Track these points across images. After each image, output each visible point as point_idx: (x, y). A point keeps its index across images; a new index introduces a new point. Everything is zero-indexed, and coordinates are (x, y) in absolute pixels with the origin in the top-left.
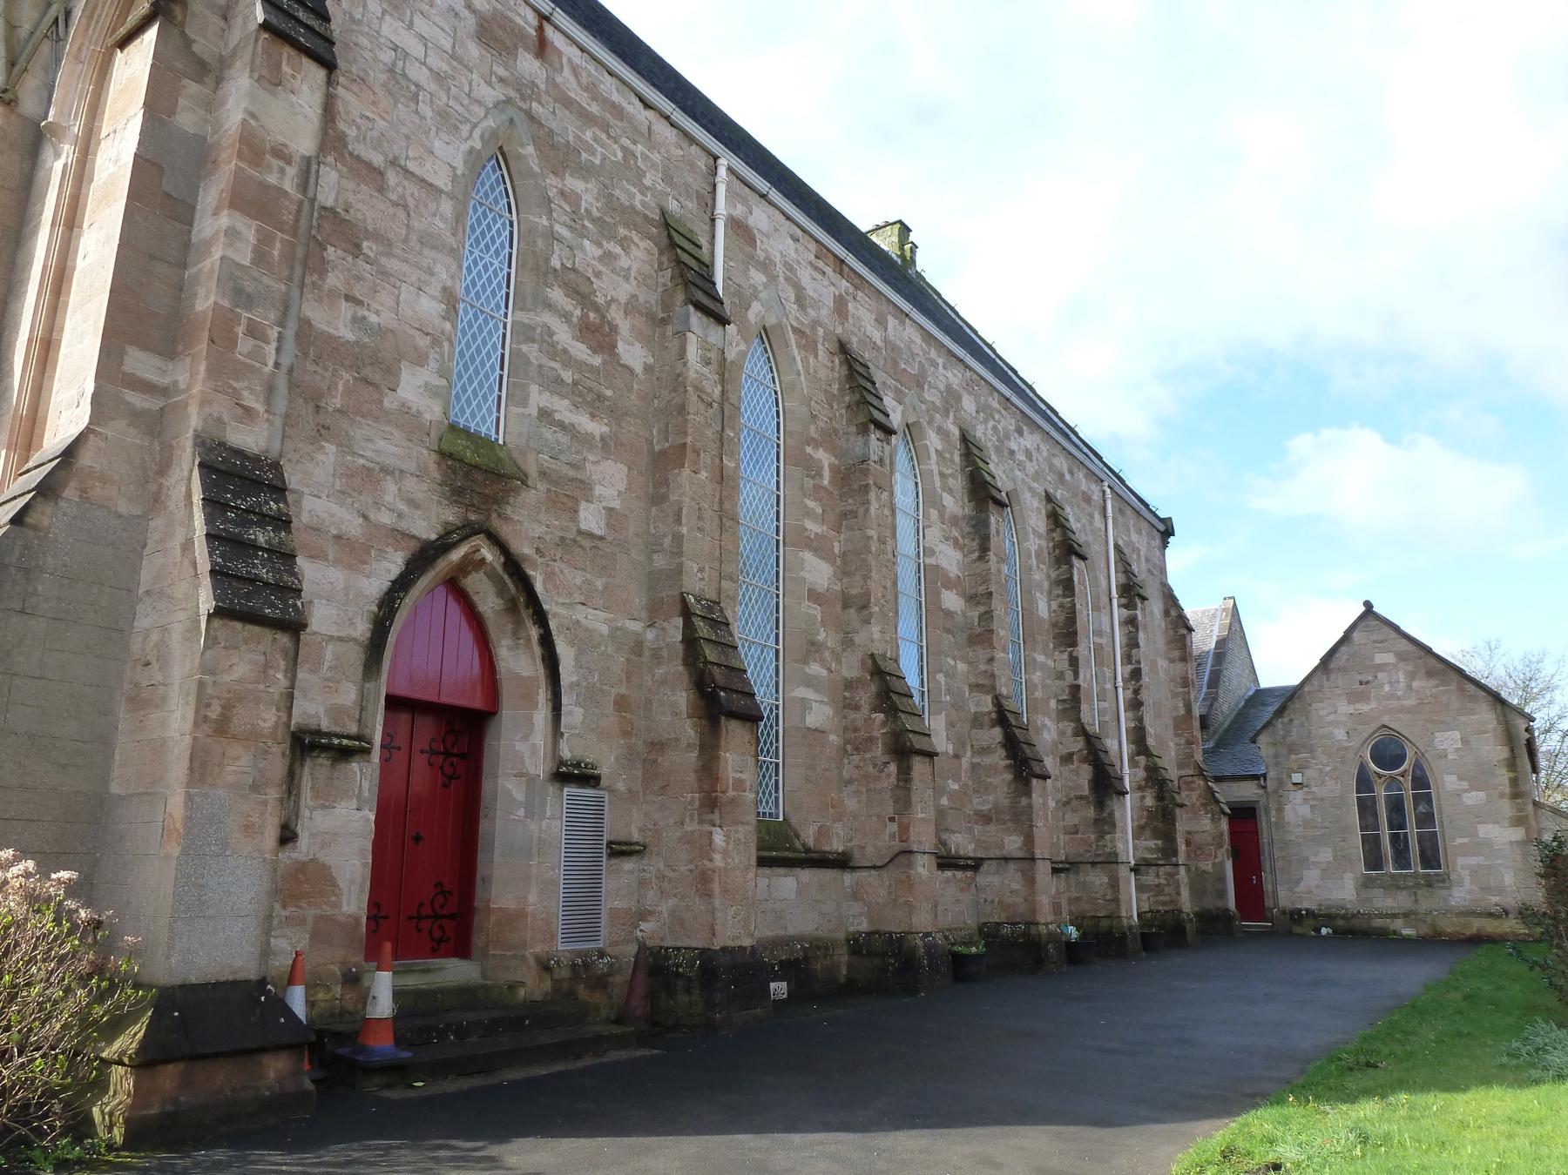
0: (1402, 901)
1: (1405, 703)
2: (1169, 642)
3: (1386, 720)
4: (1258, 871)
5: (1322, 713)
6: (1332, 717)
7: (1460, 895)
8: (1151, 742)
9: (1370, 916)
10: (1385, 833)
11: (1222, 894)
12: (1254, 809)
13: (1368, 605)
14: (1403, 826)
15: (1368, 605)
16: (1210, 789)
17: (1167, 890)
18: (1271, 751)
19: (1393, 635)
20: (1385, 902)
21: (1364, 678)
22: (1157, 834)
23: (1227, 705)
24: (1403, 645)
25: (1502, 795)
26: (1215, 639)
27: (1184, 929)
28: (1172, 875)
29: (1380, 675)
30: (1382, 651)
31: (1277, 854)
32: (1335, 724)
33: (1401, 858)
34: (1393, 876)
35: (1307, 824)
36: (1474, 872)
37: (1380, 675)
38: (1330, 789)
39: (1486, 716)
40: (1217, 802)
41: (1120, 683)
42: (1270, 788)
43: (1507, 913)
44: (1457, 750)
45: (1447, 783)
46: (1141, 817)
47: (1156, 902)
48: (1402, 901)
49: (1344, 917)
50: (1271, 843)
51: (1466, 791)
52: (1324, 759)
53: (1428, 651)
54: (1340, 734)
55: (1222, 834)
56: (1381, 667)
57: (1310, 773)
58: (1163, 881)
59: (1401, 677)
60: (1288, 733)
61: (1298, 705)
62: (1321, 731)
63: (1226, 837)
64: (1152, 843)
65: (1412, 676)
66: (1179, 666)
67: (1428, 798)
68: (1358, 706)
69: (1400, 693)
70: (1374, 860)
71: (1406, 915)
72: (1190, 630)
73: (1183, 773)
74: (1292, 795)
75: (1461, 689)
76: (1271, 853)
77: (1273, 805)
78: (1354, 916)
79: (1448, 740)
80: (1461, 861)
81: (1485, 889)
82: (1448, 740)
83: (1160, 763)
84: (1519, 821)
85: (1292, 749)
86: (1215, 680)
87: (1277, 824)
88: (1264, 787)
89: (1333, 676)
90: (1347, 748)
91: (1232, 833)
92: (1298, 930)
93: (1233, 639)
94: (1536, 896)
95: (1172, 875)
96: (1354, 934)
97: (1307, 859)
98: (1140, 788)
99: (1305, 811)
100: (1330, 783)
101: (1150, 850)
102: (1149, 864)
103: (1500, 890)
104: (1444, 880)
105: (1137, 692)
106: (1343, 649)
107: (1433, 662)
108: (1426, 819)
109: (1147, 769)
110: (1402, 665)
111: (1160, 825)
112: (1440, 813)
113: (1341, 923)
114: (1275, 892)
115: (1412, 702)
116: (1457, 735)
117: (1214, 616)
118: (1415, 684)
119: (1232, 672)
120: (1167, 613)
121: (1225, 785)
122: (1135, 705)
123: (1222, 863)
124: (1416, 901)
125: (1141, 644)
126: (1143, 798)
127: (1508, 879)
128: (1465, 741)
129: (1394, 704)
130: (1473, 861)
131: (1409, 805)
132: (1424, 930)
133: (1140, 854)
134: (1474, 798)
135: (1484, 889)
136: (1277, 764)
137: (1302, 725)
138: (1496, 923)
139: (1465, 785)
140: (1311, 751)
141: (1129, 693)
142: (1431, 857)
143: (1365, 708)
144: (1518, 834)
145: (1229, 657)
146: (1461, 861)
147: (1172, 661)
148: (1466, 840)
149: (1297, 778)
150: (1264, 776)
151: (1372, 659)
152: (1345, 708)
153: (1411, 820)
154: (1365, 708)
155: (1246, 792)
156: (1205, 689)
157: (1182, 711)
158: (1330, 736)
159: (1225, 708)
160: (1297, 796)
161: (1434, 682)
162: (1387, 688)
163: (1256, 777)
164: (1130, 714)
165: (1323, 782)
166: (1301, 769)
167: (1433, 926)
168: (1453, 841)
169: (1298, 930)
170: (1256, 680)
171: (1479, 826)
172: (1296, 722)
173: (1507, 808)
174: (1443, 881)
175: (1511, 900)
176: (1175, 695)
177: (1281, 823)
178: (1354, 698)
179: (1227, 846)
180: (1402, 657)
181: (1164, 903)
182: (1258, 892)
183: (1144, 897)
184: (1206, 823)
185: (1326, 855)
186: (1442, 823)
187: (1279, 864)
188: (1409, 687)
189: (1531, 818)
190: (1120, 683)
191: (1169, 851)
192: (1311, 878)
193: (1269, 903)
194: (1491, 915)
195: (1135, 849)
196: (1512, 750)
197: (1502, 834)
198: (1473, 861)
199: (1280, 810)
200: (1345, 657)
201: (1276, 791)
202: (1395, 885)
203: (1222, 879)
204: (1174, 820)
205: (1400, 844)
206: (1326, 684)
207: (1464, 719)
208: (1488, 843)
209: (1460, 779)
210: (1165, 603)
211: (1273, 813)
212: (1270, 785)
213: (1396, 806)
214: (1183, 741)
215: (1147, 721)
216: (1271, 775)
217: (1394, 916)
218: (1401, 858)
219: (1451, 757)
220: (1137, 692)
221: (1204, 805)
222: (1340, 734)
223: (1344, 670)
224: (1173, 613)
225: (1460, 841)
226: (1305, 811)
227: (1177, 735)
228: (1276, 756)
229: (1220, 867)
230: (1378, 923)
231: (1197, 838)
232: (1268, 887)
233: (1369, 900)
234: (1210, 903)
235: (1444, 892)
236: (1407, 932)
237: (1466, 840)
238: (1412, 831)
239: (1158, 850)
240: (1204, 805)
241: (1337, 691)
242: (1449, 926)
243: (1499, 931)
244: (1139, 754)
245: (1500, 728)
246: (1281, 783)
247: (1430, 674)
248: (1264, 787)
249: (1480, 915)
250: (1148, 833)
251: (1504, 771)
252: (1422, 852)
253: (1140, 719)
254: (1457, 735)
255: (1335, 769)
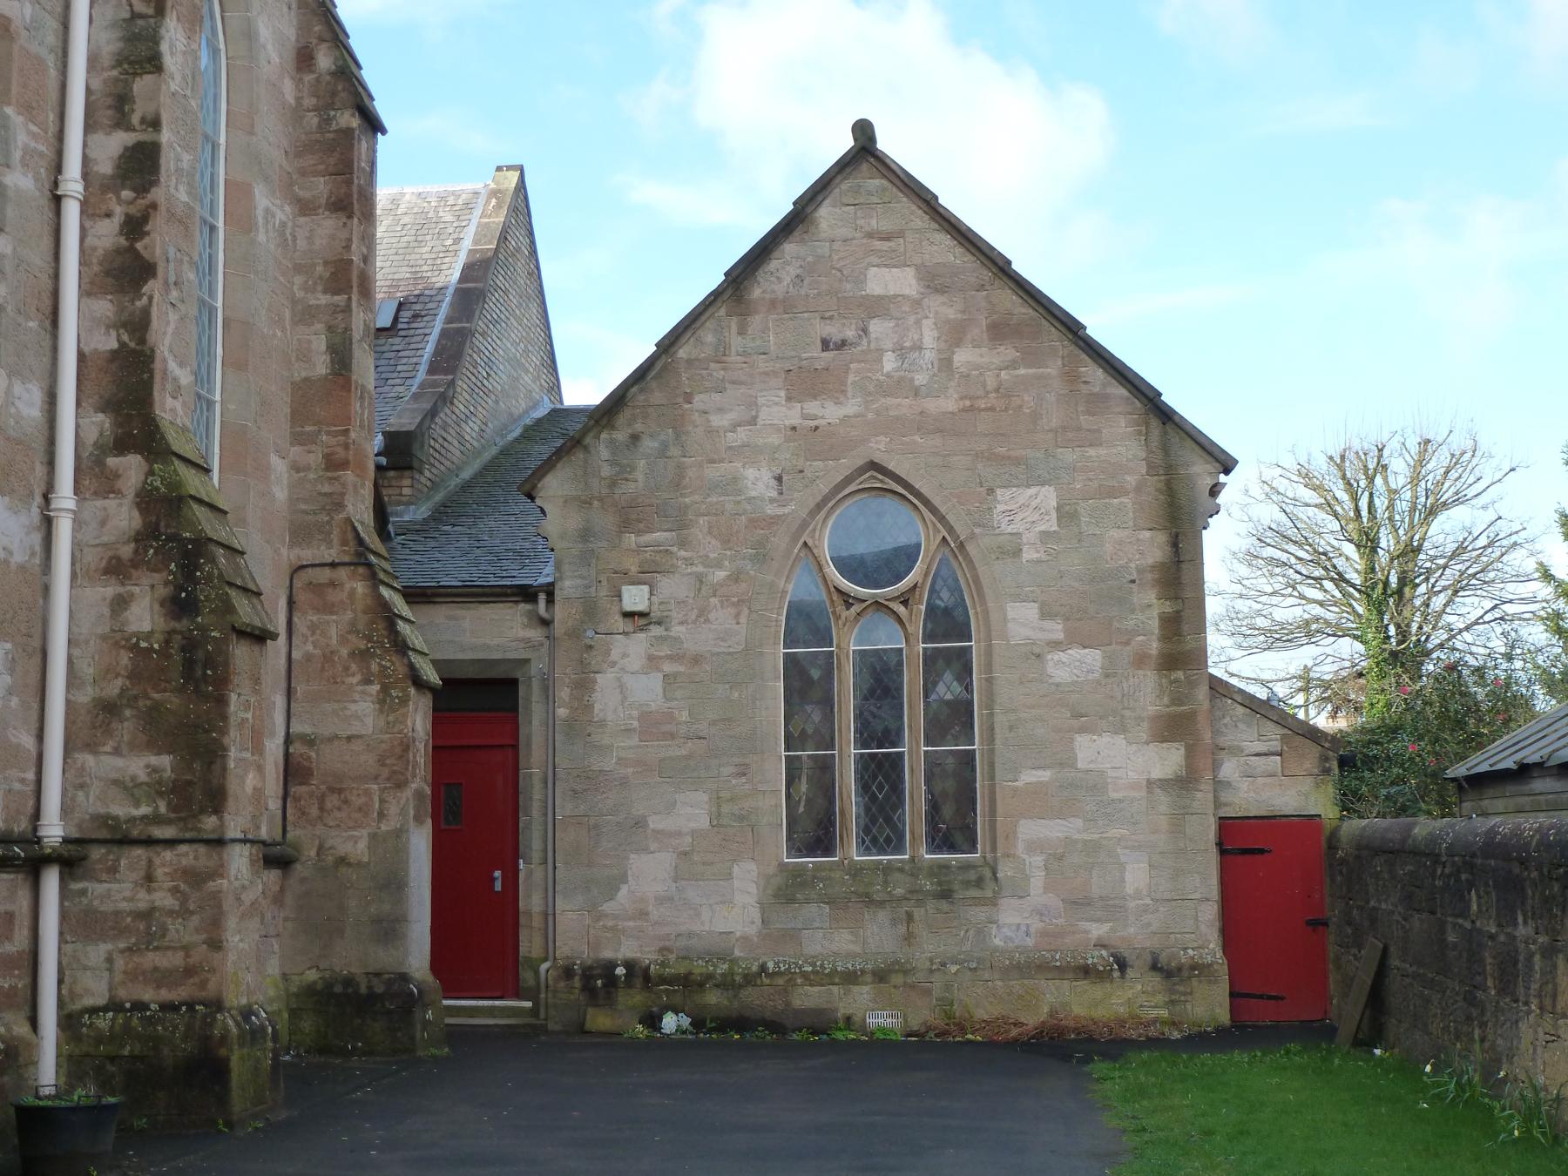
0: (876, 937)
1: (932, 405)
2: (301, 150)
3: (878, 448)
4: (509, 854)
5: (717, 421)
6: (742, 435)
7: (1016, 921)
8: (170, 409)
9: (790, 978)
10: (848, 754)
11: (390, 929)
12: (512, 684)
13: (864, 131)
14: (891, 736)
15: (864, 131)
16: (385, 606)
17: (174, 926)
18: (574, 521)
19: (920, 220)
20: (830, 939)
21: (833, 331)
22: (158, 731)
23: (474, 429)
24: (943, 249)
25: (1140, 660)
26: (462, 259)
27: (219, 1071)
28: (196, 878)
29: (876, 327)
30: (893, 261)
31: (565, 807)
32: (748, 453)
33: (882, 826)
34: (856, 871)
35: (652, 726)
36: (1056, 857)
37: (876, 327)
38: (722, 630)
39: (1123, 445)
40: (401, 647)
41: (72, 183)
42: (558, 629)
43: (1122, 965)
44: (1046, 536)
45: (1015, 621)
46: (108, 673)
47: (133, 976)
48: (876, 937)
49: (727, 984)
50: (550, 779)
51: (1056, 645)
52: (712, 548)
53: (1000, 267)
54: (758, 481)
55: (406, 746)
56: (878, 306)
57: (673, 587)
58: (163, 899)
59: (929, 337)
60: (623, 471)
61: (657, 397)
62: (713, 473)
63: (421, 756)
64: (137, 766)
65: (955, 335)
66: (328, 224)
67: (961, 664)
68: (813, 407)
69: (920, 379)
70: (815, 834)
71: (880, 976)
72: (374, 125)
73: (308, 555)
74: (619, 645)
75: (1071, 377)
76: (549, 808)
77: (565, 673)
78: (750, 979)
79: (1027, 511)
80: (1029, 829)
81: (1079, 903)
82: (1027, 511)
83: (192, 482)
84: (1174, 727)
85: (630, 518)
86: (450, 356)
87: (570, 723)
88: (546, 623)
89: (756, 322)
90: (775, 520)
91: (440, 751)
92: (600, 1020)
93: (504, 268)
94: (1198, 929)
95: (196, 878)
96: (745, 1029)
97: (640, 823)
98: (116, 569)
99: (647, 690)
100: (721, 617)
101: (129, 788)
102: (121, 838)
103: (1112, 907)
104: (985, 880)
105: (135, 227)
106: (789, 248)
107: (1008, 300)
108: (954, 718)
109: (146, 500)
110: (935, 303)
111: (173, 701)
112: (990, 704)
113: (713, 998)
114: (549, 915)
115: (949, 404)
116: (1048, 497)
117: (468, 207)
118: (962, 357)
119: (498, 344)
120: (304, 59)
121: (439, 614)
122: (126, 272)
123: (399, 833)
124: (909, 938)
125: (170, 61)
126: (120, 604)
127: (1136, 876)
128: (1066, 514)
129: (902, 405)
130: (1053, 830)
131: (912, 680)
132: (922, 1014)
133: (91, 803)
134: (1075, 665)
135: (1079, 903)
136: (586, 558)
137: (663, 453)
138: (1096, 991)
139: (1056, 630)
140: (681, 525)
141: (108, 233)
142: (955, 822)
143: (829, 412)
144: (1167, 760)
145: (492, 305)
146: (1029, 829)
147: (305, 208)
148: (1045, 775)
149: (635, 597)
150: (549, 590)
151: (861, 281)
152: (778, 412)
153: (914, 716)
154: (829, 412)
155: (490, 634)
156: (421, 374)
157: (321, 366)
158: (732, 485)
159: (471, 430)
160: (631, 649)
161: (1008, 352)
162: (889, 363)
163: (526, 594)
164: (104, 307)
165: (703, 613)
166: (647, 574)
167: (946, 1005)
168: (1015, 776)
169: (600, 1020)
170: (555, 388)
171: (1081, 741)
172: (648, 444)
173: (1147, 693)
174: (979, 883)
175: (1136, 934)
176: (305, 315)
177: (582, 724)
178: (806, 383)
179: (420, 780)
180: (934, 281)
181: (160, 978)
182: (502, 915)
183: (96, 953)
184: (362, 712)
185: (691, 812)
186: (990, 730)
187: (565, 839)
188: (946, 364)
189: (1202, 721)
190: (72, 183)
191: (198, 791)
192: (649, 874)
193: (529, 944)
194: (1086, 971)
195: (74, 782)
196: (1175, 544)
197: (1128, 761)
198: (1053, 830)
199: (584, 686)
200: (793, 271)
201: (575, 634)
202: (863, 895)
203: (394, 884)
204: (222, 683)
205: (882, 776)
206: (736, 342)
207: (1068, 456)
208: (1095, 784)
209: (1046, 614)
210: (303, 28)
211: (564, 693)
212: (562, 614)
213: (881, 680)
214: (315, 458)
215: (166, 335)
216: (568, 587)
217: (851, 978)
218: (882, 826)
219: (1028, 554)
220: (135, 227)
221: (363, 656)
222: (758, 481)
223: (785, 306)
224: (325, 61)
225: (1029, 777)
226: (647, 690)
227: (298, 439)
228: (585, 534)
229: (392, 846)
230: (808, 997)
231: (327, 760)
232: (531, 901)
233: (791, 936)
234: (353, 958)
235: (979, 914)
236: (881, 1020)
237: (1045, 775)
238: (914, 750)
239: (157, 788)
240: (363, 656)
241: (762, 364)
242: (984, 1003)
243: (1100, 1013)
244: (122, 445)
245: (1154, 483)
246: (590, 610)
247: (999, 331)
248: (546, 623)
249: (1061, 971)
250: (127, 728)
251: (1151, 596)
252: (934, 808)
253: (138, 325)
254: (1048, 497)
255: (736, 577)
